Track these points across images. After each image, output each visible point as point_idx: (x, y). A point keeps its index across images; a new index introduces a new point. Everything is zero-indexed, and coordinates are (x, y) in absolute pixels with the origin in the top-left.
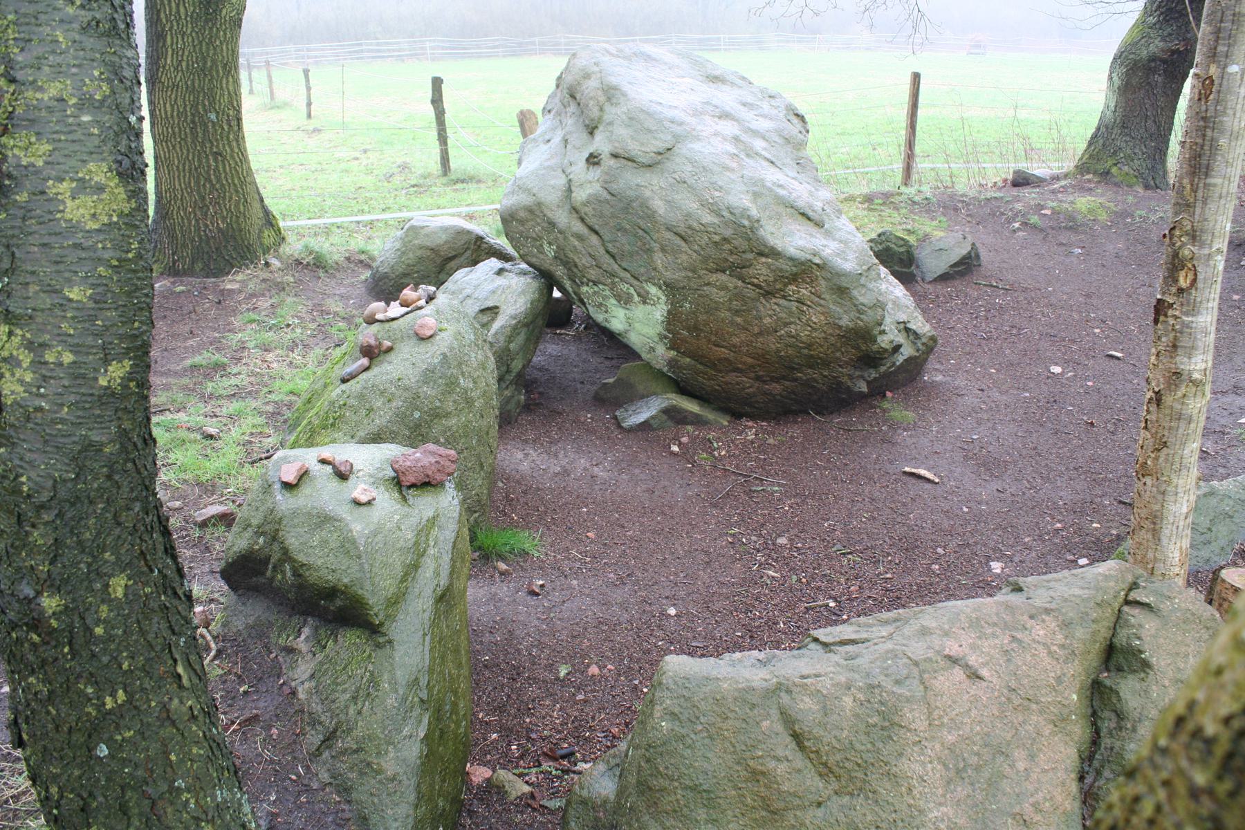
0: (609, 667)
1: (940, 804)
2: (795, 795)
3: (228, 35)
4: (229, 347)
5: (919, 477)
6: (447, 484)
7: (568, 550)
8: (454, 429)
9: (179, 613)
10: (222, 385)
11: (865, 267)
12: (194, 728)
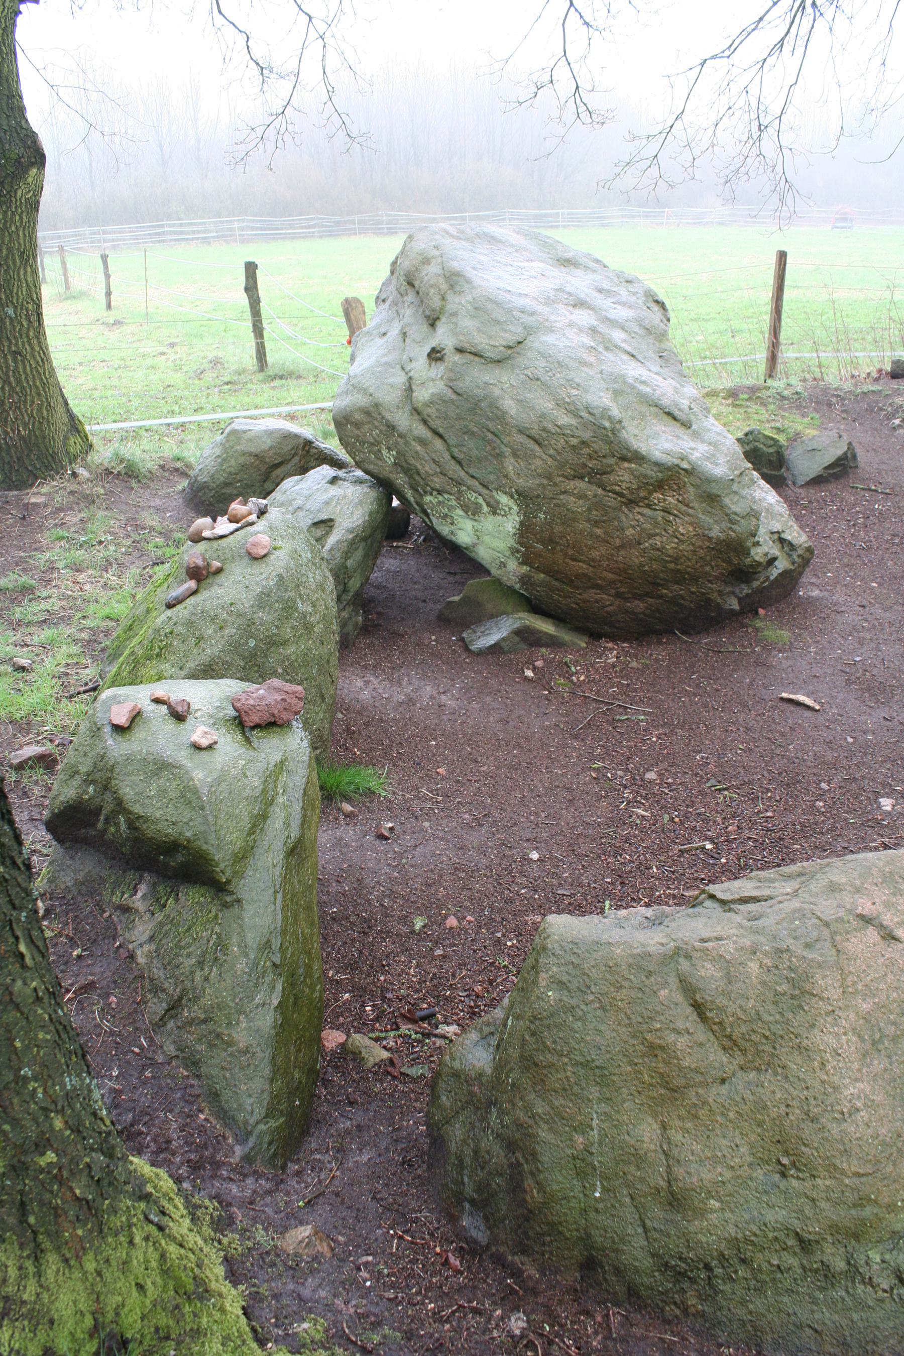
0: (469, 918)
1: (856, 1080)
2: (697, 1071)
3: (25, 220)
4: (36, 568)
6: (294, 723)
7: (416, 788)
8: (293, 657)
9: (19, 885)
10: (33, 610)
11: (737, 472)
12: (40, 1011)
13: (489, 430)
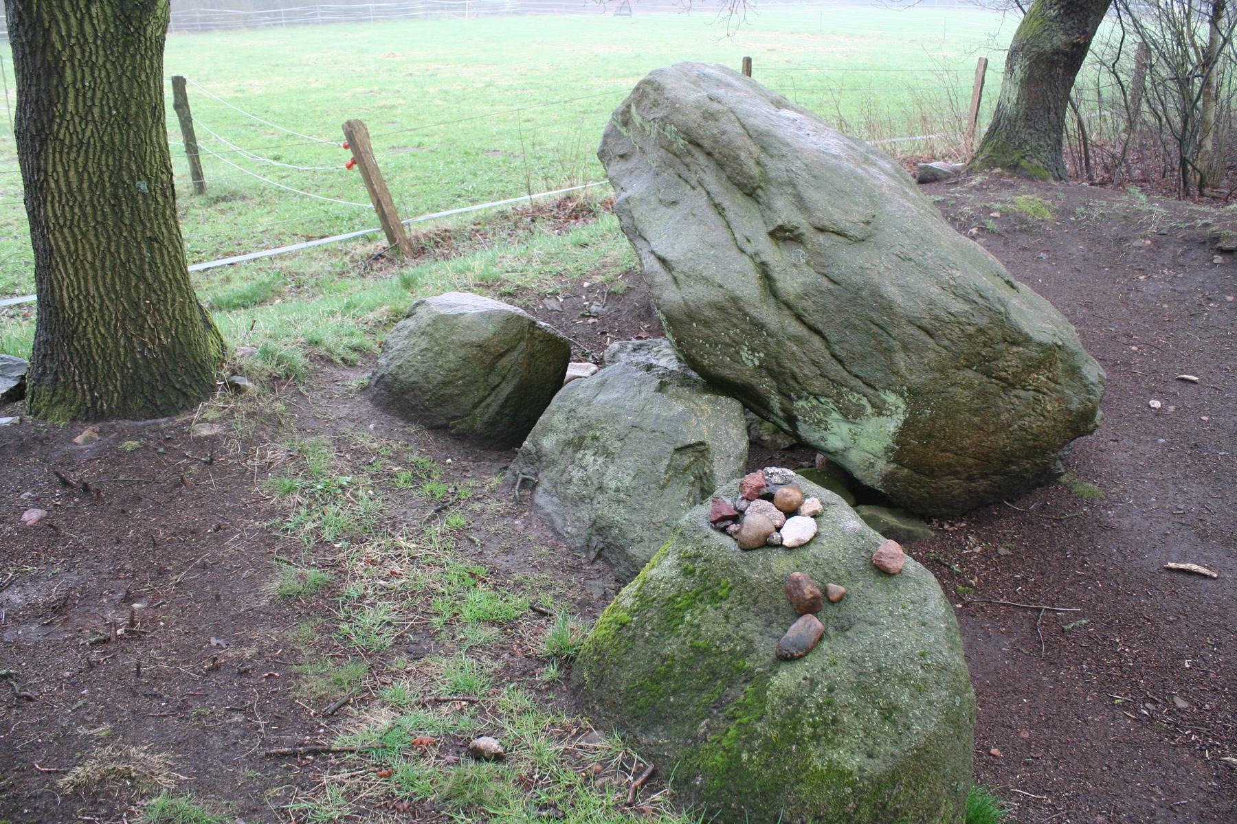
5: (1190, 573)
13: (873, 323)
